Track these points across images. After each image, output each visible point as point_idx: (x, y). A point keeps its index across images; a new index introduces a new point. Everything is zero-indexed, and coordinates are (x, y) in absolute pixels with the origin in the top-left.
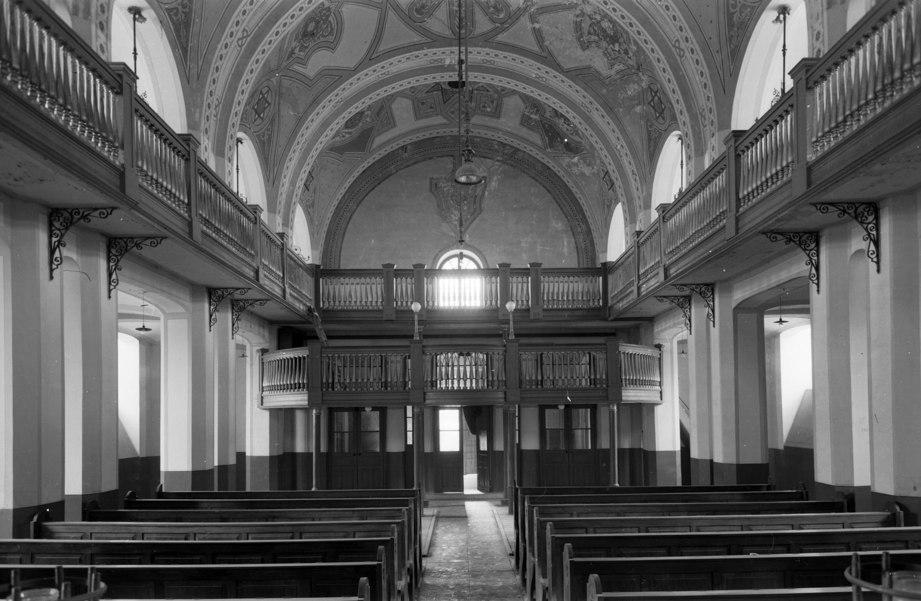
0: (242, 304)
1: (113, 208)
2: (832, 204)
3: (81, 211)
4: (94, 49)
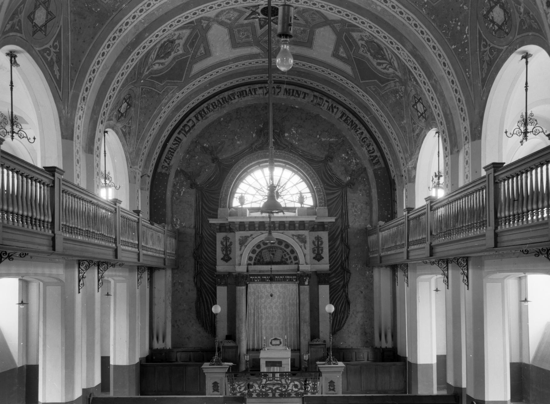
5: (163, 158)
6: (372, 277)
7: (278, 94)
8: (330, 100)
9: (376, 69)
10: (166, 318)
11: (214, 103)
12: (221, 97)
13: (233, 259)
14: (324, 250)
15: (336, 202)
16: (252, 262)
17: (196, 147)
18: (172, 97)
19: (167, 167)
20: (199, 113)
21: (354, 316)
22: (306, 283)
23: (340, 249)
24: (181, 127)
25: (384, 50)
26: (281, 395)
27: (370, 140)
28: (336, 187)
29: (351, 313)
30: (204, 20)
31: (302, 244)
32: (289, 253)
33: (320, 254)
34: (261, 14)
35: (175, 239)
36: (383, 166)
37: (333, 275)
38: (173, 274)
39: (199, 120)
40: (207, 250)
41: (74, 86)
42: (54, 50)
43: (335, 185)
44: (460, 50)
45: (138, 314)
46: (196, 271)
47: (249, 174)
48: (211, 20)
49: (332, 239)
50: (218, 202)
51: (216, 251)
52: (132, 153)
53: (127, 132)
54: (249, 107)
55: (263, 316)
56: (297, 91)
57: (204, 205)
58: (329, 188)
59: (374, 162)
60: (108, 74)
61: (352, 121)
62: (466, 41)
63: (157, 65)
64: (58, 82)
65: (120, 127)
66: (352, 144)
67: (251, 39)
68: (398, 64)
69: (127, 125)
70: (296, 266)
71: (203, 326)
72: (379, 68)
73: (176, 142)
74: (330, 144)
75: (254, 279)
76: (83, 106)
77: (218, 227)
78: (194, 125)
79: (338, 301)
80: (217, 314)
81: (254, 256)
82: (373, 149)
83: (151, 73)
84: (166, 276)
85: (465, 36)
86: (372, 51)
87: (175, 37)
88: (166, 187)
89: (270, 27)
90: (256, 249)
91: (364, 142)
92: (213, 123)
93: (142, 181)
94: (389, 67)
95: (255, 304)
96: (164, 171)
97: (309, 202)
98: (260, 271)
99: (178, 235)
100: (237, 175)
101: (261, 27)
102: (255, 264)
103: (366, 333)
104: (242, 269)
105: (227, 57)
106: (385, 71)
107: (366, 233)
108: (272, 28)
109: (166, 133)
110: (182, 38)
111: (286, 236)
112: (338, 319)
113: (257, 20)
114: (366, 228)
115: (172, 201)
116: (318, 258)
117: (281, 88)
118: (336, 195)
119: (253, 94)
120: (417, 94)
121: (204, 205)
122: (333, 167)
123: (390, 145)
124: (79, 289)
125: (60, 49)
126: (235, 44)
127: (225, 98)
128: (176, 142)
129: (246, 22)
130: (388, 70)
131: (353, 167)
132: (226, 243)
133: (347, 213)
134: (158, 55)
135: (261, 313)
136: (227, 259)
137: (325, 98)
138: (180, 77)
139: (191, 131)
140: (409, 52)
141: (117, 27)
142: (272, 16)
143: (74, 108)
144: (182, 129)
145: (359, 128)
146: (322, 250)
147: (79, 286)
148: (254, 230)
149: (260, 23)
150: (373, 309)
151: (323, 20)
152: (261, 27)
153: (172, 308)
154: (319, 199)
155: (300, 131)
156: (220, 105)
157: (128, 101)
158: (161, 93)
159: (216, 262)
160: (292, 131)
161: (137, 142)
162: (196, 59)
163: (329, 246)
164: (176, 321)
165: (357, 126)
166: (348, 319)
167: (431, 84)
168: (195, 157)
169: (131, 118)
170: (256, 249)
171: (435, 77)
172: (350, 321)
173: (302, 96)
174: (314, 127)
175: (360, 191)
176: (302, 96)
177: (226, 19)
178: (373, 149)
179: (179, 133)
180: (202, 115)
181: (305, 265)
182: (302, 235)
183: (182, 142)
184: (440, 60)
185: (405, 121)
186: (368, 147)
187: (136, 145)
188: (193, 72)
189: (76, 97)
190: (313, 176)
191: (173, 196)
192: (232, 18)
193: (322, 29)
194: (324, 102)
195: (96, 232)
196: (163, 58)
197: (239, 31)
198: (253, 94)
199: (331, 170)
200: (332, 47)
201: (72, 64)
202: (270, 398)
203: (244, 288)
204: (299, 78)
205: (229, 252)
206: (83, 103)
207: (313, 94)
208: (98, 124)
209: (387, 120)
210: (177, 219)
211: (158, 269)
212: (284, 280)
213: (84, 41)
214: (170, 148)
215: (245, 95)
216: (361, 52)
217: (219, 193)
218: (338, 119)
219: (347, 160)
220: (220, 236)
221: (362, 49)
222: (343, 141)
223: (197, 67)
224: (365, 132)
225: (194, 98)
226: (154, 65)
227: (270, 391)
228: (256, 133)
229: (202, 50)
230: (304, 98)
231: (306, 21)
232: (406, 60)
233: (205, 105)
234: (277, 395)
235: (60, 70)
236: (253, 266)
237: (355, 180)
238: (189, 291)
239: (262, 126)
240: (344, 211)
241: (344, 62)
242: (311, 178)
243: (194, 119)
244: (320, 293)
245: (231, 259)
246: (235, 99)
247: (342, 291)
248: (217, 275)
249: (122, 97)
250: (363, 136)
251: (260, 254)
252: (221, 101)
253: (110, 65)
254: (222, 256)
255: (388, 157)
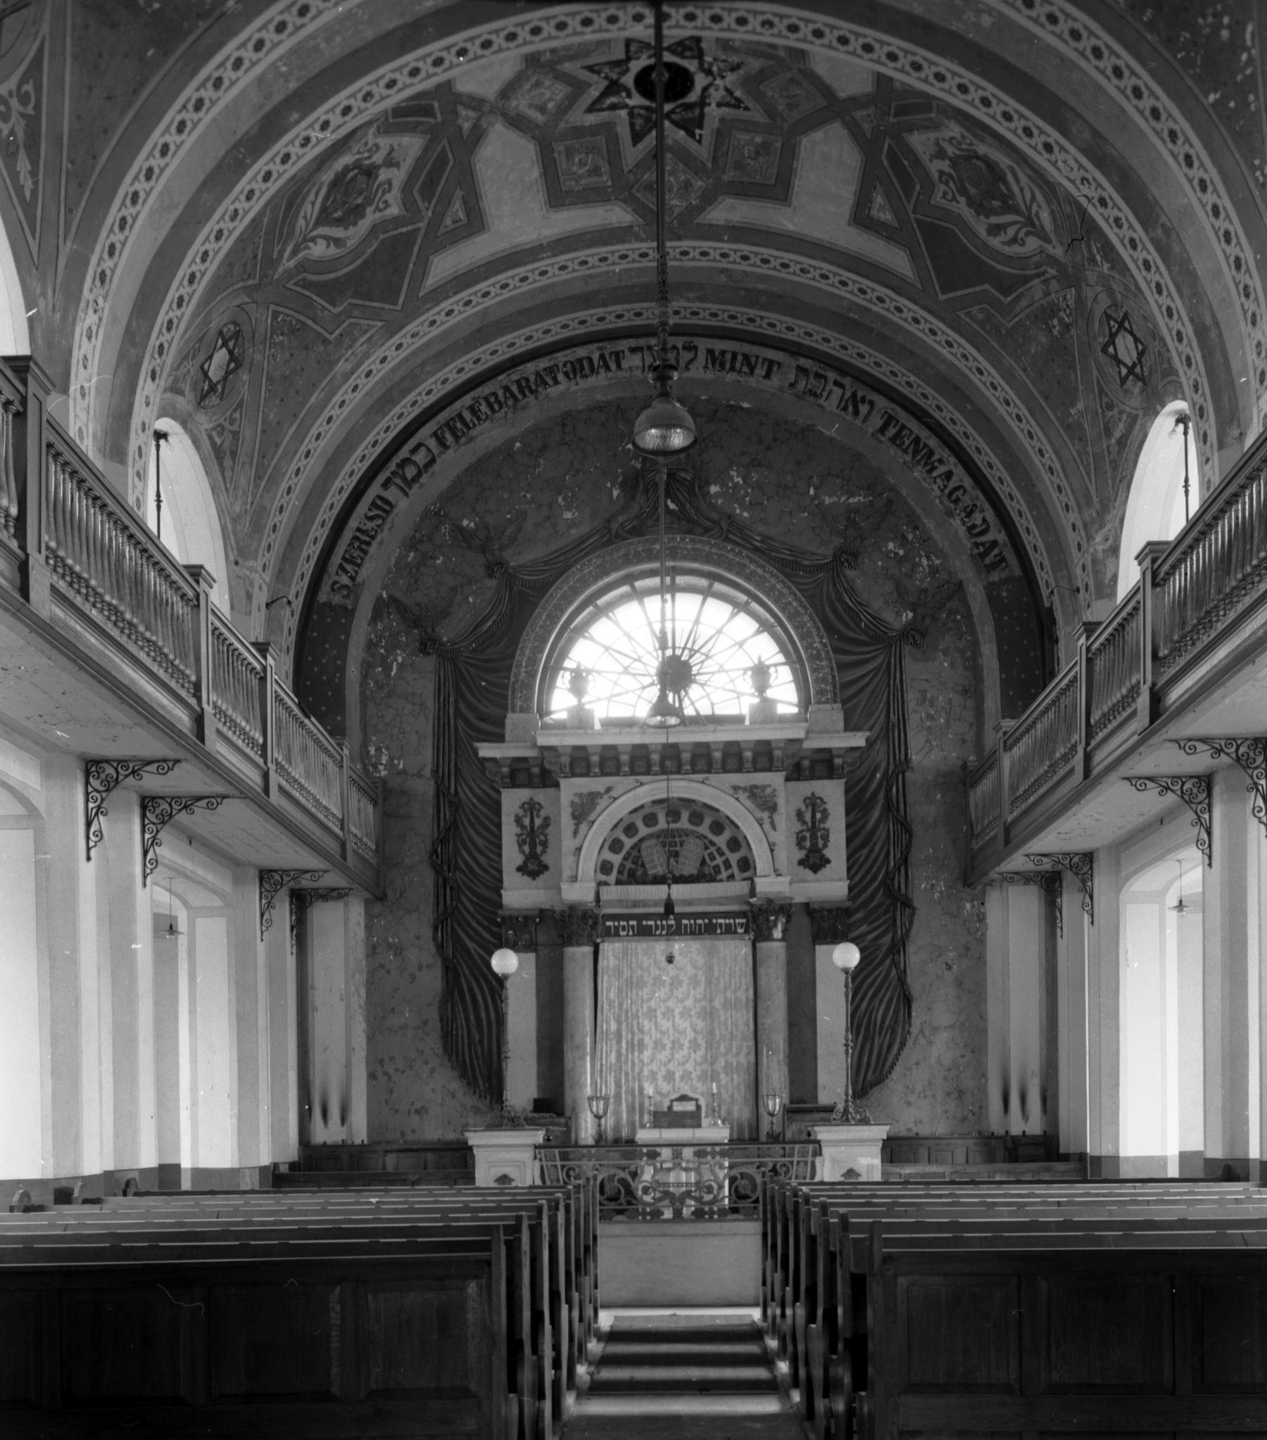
0: (277, 877)
1: (177, 761)
2: (1151, 779)
3: (131, 765)
4: (72, 434)
5: (336, 559)
6: (981, 918)
7: (687, 368)
8: (847, 381)
9: (986, 247)
10: (350, 1050)
11: (495, 394)
12: (515, 377)
13: (552, 869)
14: (832, 838)
15: (869, 689)
16: (613, 877)
17: (437, 528)
18: (367, 355)
19: (346, 587)
20: (447, 424)
21: (922, 1041)
22: (777, 933)
23: (881, 834)
24: (392, 466)
25: (1010, 177)
26: (699, 1215)
27: (973, 494)
28: (865, 644)
29: (914, 1030)
30: (467, 107)
31: (766, 815)
32: (725, 849)
33: (819, 851)
34: (634, 92)
35: (375, 804)
36: (1017, 572)
37: (859, 915)
38: (369, 916)
39: (446, 447)
40: (471, 839)
41: (73, 229)
42: (21, 108)
43: (864, 638)
44: (1232, 104)
45: (263, 1020)
46: (441, 908)
47: (601, 612)
48: (486, 108)
49: (856, 805)
50: (506, 697)
51: (500, 847)
52: (239, 517)
53: (226, 446)
54: (600, 407)
55: (647, 1040)
56: (746, 357)
57: (462, 705)
58: (846, 647)
59: (988, 561)
60: (176, 226)
61: (917, 440)
62: (1249, 71)
63: (322, 243)
64: (29, 208)
65: (208, 426)
66: (919, 511)
67: (606, 180)
68: (1052, 213)
69: (226, 424)
70: (746, 885)
71: (463, 1075)
72: (995, 242)
73: (375, 512)
74: (851, 510)
75: (617, 928)
76: (100, 301)
77: (505, 770)
78: (432, 461)
79: (875, 995)
80: (506, 977)
81: (616, 859)
82: (984, 520)
83: (303, 267)
84: (346, 920)
85: (1244, 57)
86: (972, 191)
87: (378, 158)
88: (344, 647)
89: (661, 137)
90: (623, 837)
91: (957, 501)
92: (489, 457)
93: (269, 620)
94: (1027, 234)
95: (621, 1005)
96: (337, 599)
97: (785, 693)
98: (636, 904)
99: (383, 795)
100: (563, 612)
101: (637, 137)
102: (619, 882)
103: (961, 1093)
104: (579, 892)
105: (534, 236)
106: (1016, 249)
107: (964, 778)
108: (669, 142)
109: (345, 482)
110: (397, 165)
111: (713, 791)
112: (876, 1049)
113: (623, 113)
114: (964, 766)
115: (362, 693)
116: (814, 861)
117: (696, 348)
118: (870, 666)
119: (613, 366)
120: (1115, 305)
121: (462, 705)
122: (859, 583)
123: (1036, 501)
124: (88, 849)
125: (38, 107)
126: (557, 197)
127: (527, 380)
128: (375, 512)
129: (591, 119)
130: (1023, 244)
131: (921, 579)
132: (532, 821)
133: (903, 720)
134: (324, 209)
135: (641, 1031)
136: (534, 867)
137: (832, 376)
138: (390, 293)
139: (423, 479)
140: (1082, 151)
141: (208, 69)
142: (668, 99)
143: (72, 296)
144: (394, 473)
145: (940, 461)
146: (826, 838)
147: (88, 838)
148: (617, 773)
149: (632, 125)
150: (983, 1017)
151: (822, 102)
152: (637, 137)
153: (367, 1021)
154: (816, 681)
155: (755, 476)
156: (510, 402)
157: (231, 344)
158: (332, 337)
159: (501, 881)
160: (731, 478)
161: (257, 486)
162: (440, 240)
163: (848, 827)
164: (381, 1062)
165: (931, 453)
166: (906, 1049)
167: (1152, 240)
168: (433, 558)
169: (240, 406)
170: (623, 837)
171: (1163, 219)
172: (911, 1054)
173: (760, 371)
174: (799, 463)
175: (945, 652)
176: (760, 371)
177: (530, 106)
178: (984, 520)
179: (385, 485)
180: (457, 430)
181: (773, 879)
182: (764, 787)
183: (396, 511)
184: (1175, 150)
185: (1080, 406)
186: (969, 515)
187: (254, 496)
188: (431, 281)
189: (79, 264)
190: (797, 612)
191: (365, 676)
192: (550, 105)
193: (818, 135)
194: (830, 386)
195: (141, 628)
196: (338, 222)
197: (569, 153)
198: (613, 366)
199: (852, 591)
200: (848, 194)
201: (73, 162)
202: (667, 1221)
203: (587, 950)
204: (752, 312)
205: (539, 849)
206: (99, 291)
207: (793, 363)
208: (141, 382)
209: (1024, 412)
210: (378, 749)
212: (710, 930)
213: (109, 98)
214: (358, 529)
215: (587, 371)
216: (938, 199)
217: (509, 668)
218: (873, 435)
219: (901, 561)
220: (512, 800)
221: (943, 187)
222: (890, 502)
223: (443, 266)
224: (959, 471)
225: (433, 374)
226: (313, 240)
227: (667, 1202)
228: (623, 486)
229: (457, 208)
230: (768, 376)
231: (771, 112)
232: (1072, 182)
233: (467, 400)
234: (686, 1212)
235: (34, 173)
236: (613, 888)
237: (928, 621)
238: (420, 968)
239: (638, 466)
240: (893, 718)
241: (889, 238)
242: (790, 618)
243: (432, 443)
244: (818, 970)
245: (546, 868)
246: (556, 382)
247: (887, 963)
248: (503, 918)
249: (214, 325)
250: (953, 483)
251: (635, 856)
252: (514, 388)
253: (183, 200)
254: (519, 860)
255: (1033, 539)
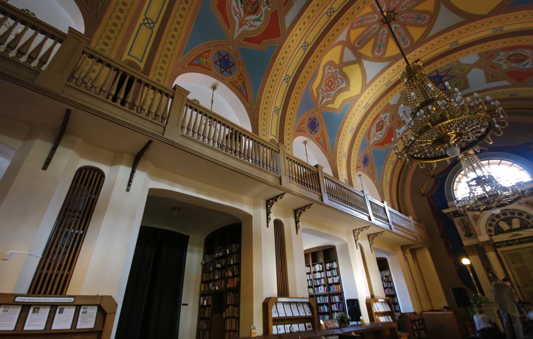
81: (492, 228)
125: (243, 80)
134: (376, 130)
136: (470, 234)
211: (418, 249)
220: (456, 220)
254: (464, 233)
